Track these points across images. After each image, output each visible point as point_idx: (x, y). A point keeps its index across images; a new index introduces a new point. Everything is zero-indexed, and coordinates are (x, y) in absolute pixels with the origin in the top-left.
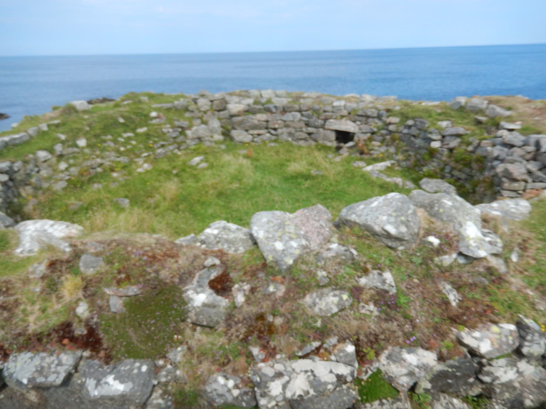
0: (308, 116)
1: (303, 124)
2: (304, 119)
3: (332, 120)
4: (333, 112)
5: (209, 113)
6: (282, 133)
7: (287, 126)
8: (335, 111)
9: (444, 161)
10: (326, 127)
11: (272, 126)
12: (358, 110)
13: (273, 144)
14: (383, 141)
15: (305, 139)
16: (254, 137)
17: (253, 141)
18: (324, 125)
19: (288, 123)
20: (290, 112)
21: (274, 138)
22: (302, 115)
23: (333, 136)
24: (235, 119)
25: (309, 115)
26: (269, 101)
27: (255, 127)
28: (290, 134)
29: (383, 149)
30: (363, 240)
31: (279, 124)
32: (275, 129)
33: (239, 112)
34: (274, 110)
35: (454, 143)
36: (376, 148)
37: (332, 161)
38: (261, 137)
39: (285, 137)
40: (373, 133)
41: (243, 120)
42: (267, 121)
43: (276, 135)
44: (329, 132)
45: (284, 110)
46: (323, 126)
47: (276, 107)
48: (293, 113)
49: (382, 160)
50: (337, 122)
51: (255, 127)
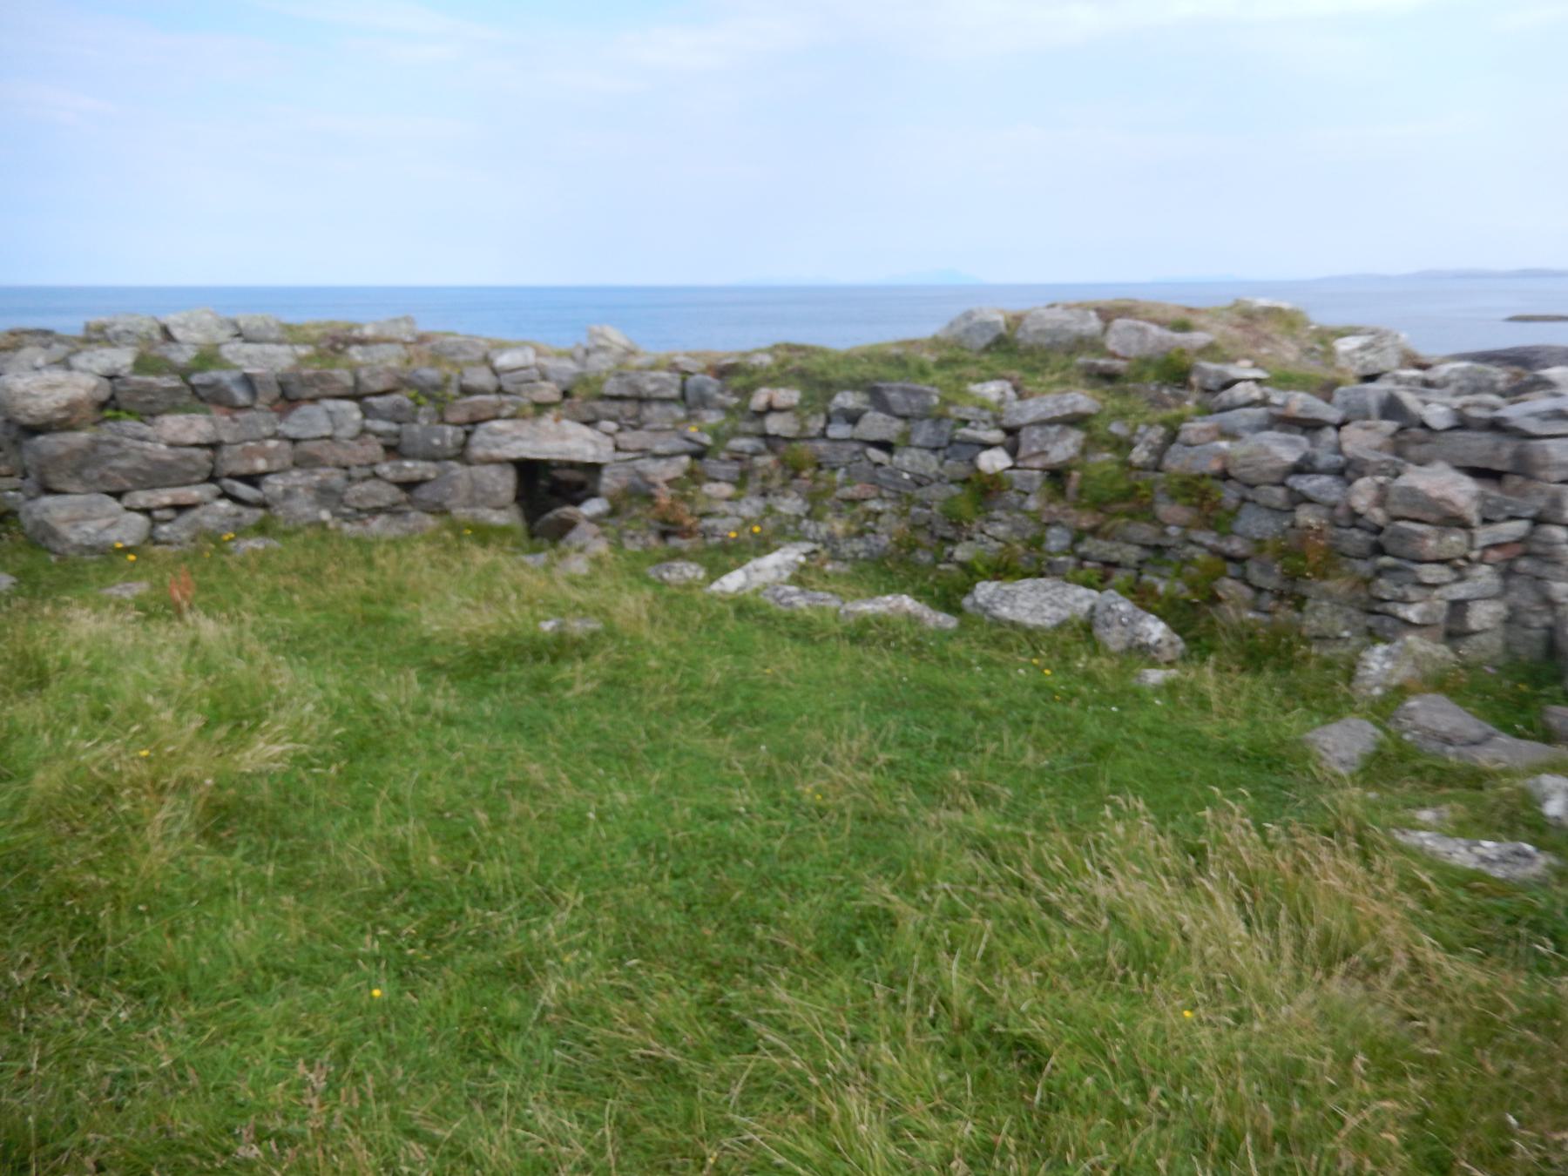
1: (374, 449)
2: (381, 426)
3: (497, 425)
4: (500, 390)
6: (288, 493)
7: (305, 462)
8: (508, 386)
9: (1035, 516)
10: (477, 451)
11: (243, 468)
13: (256, 543)
14: (741, 481)
15: (392, 510)
16: (155, 522)
17: (152, 539)
18: (464, 445)
19: (307, 447)
20: (314, 400)
21: (251, 516)
22: (367, 412)
23: (505, 484)
24: (47, 443)
25: (400, 408)
26: (209, 358)
27: (157, 476)
28: (325, 494)
29: (750, 506)
31: (267, 455)
32: (253, 479)
33: (72, 406)
34: (242, 397)
35: (1064, 448)
36: (723, 507)
38: (195, 513)
39: (303, 507)
40: (699, 454)
41: (94, 445)
42: (215, 446)
43: (264, 505)
44: (492, 471)
45: (288, 397)
46: (462, 454)
47: (248, 381)
48: (331, 404)
49: (764, 546)
50: (524, 428)
51: (157, 476)
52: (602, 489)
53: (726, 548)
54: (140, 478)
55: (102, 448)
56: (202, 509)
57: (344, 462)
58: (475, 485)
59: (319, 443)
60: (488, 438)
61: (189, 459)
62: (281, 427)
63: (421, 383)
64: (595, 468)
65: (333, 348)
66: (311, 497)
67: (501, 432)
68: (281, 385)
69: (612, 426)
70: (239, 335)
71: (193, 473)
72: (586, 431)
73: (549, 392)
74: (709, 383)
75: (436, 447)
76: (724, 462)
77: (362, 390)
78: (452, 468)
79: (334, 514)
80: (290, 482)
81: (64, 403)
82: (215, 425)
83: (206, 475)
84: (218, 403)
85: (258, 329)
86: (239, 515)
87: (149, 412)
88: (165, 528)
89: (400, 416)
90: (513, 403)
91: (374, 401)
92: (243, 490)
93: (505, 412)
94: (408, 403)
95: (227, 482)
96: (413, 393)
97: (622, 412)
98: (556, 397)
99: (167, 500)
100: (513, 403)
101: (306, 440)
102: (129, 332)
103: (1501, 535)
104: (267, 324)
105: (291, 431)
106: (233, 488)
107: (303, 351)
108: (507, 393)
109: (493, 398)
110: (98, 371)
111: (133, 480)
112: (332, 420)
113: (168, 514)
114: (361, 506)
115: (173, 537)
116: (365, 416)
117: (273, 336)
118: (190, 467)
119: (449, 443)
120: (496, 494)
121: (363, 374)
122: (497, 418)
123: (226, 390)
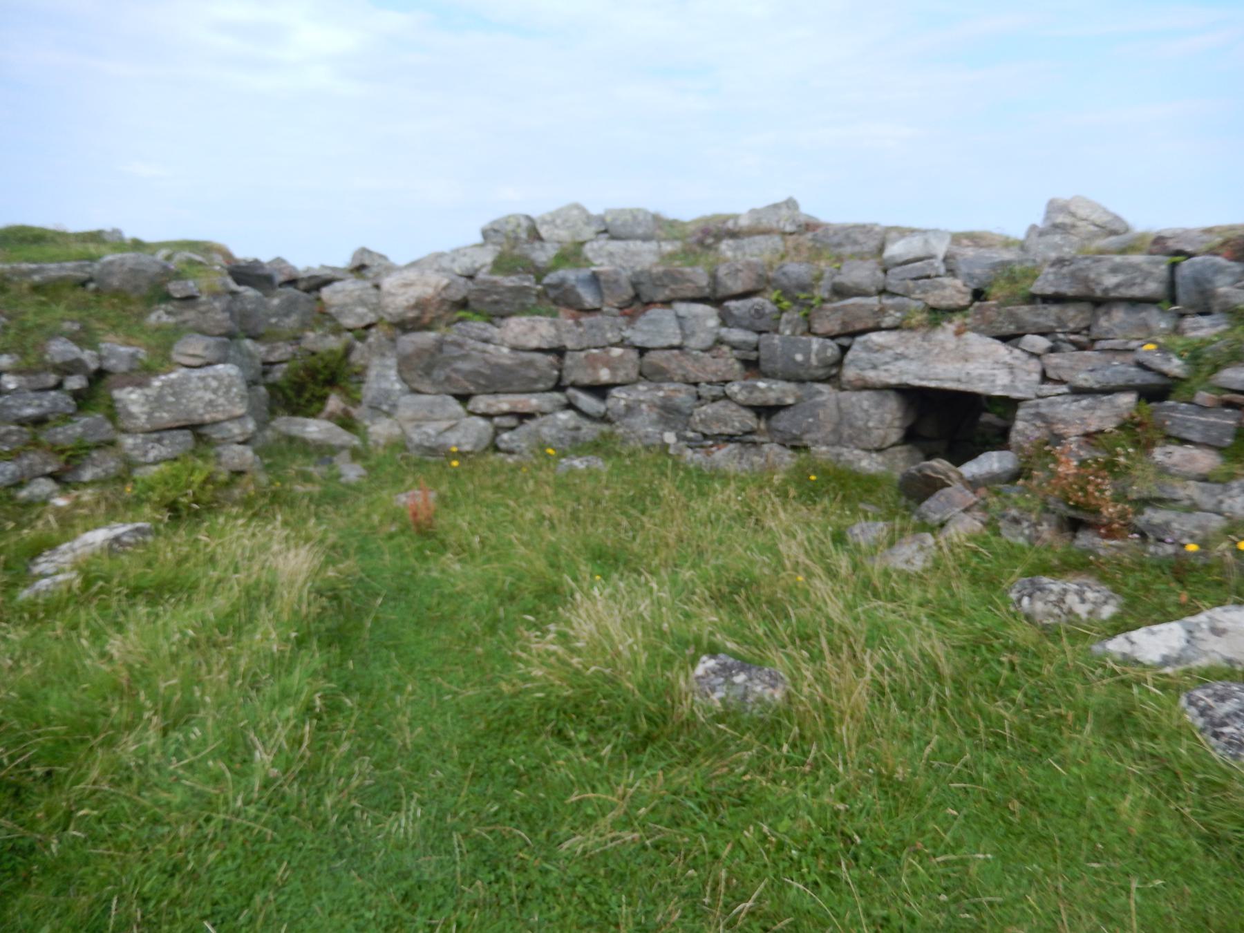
0: (762, 325)
1: (728, 363)
2: (736, 335)
3: (875, 337)
5: (374, 336)
6: (630, 410)
12: (1032, 275)
15: (743, 439)
16: (498, 430)
20: (667, 303)
21: (590, 430)
25: (760, 314)
26: (572, 254)
27: (498, 381)
28: (669, 413)
30: (955, 590)
31: (611, 364)
32: (600, 391)
33: (421, 305)
34: (589, 299)
37: (875, 568)
38: (531, 425)
39: (645, 425)
41: (440, 345)
43: (604, 419)
44: (865, 400)
46: (832, 374)
47: (595, 279)
48: (682, 308)
50: (912, 343)
51: (498, 381)
52: (1014, 437)
53: (1180, 570)
54: (482, 382)
55: (446, 348)
56: (541, 419)
57: (692, 379)
58: (843, 417)
59: (667, 353)
60: (863, 355)
61: (530, 364)
62: (627, 333)
63: (785, 281)
64: (1009, 405)
65: (701, 243)
66: (654, 416)
67: (882, 348)
68: (635, 285)
69: (1042, 343)
70: (605, 231)
71: (536, 381)
72: (1001, 350)
73: (953, 291)
74: (1219, 270)
75: (800, 365)
76: (1203, 409)
77: (721, 292)
78: (820, 393)
79: (680, 438)
80: (634, 396)
81: (412, 302)
82: (558, 329)
83: (551, 384)
84: (569, 305)
85: (624, 224)
86: (578, 429)
87: (496, 315)
88: (506, 436)
89: (761, 324)
90: (898, 308)
91: (732, 304)
92: (587, 402)
93: (888, 321)
94: (770, 307)
95: (571, 391)
96: (774, 296)
97: (1061, 322)
98: (964, 300)
99: (505, 407)
100: (898, 308)
101: (654, 349)
102: (496, 231)
103: (943, 298)
104: (635, 217)
105: (638, 339)
106: (576, 398)
107: (668, 247)
108: (894, 295)
109: (873, 301)
110: (458, 271)
111: (477, 384)
112: (681, 327)
113: (510, 421)
114: (707, 432)
115: (513, 445)
116: (724, 323)
117: (640, 231)
118: (532, 374)
119: (814, 361)
120: (868, 431)
121: (722, 271)
122: (877, 329)
123: (572, 290)
